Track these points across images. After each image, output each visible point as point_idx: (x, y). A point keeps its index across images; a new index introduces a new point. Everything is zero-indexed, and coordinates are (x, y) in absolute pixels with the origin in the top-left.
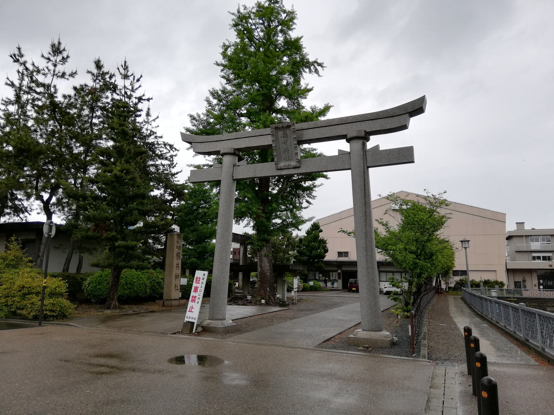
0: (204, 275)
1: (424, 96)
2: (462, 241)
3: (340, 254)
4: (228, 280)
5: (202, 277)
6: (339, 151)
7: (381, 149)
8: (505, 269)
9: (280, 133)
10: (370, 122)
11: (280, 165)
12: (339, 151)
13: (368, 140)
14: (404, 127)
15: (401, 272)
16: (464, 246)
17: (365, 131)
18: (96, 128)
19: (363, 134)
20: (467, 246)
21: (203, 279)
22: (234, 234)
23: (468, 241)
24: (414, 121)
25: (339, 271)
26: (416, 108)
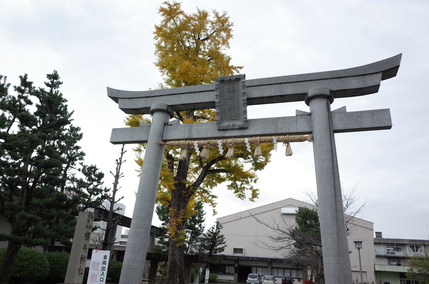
0: (105, 257)
1: (400, 55)
2: (355, 242)
3: (236, 250)
4: (323, 251)
5: (102, 260)
6: (297, 111)
7: (348, 110)
8: (374, 271)
9: (227, 87)
10: (336, 80)
11: (223, 125)
12: (297, 111)
13: (332, 102)
14: (374, 89)
15: (291, 269)
16: (357, 246)
17: (330, 90)
18: (56, 143)
19: (328, 93)
20: (360, 246)
21: (104, 263)
22: (152, 226)
23: (361, 242)
24: (385, 84)
25: (236, 265)
26: (389, 69)
